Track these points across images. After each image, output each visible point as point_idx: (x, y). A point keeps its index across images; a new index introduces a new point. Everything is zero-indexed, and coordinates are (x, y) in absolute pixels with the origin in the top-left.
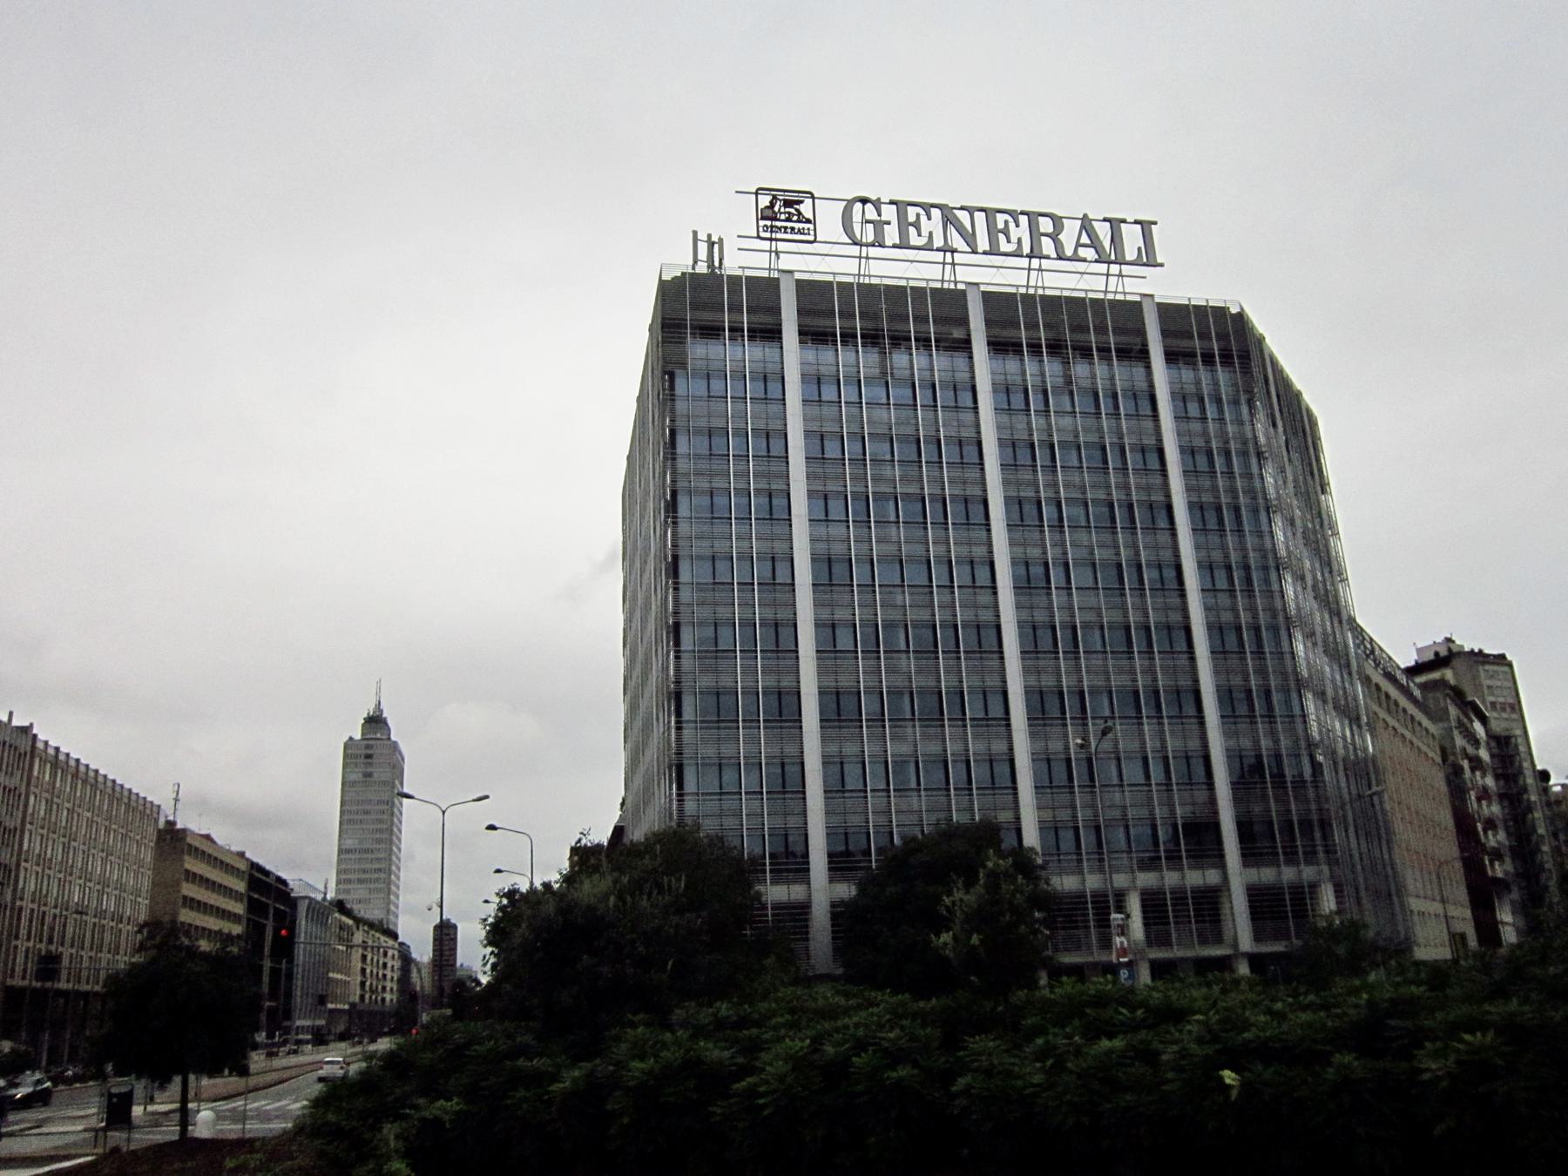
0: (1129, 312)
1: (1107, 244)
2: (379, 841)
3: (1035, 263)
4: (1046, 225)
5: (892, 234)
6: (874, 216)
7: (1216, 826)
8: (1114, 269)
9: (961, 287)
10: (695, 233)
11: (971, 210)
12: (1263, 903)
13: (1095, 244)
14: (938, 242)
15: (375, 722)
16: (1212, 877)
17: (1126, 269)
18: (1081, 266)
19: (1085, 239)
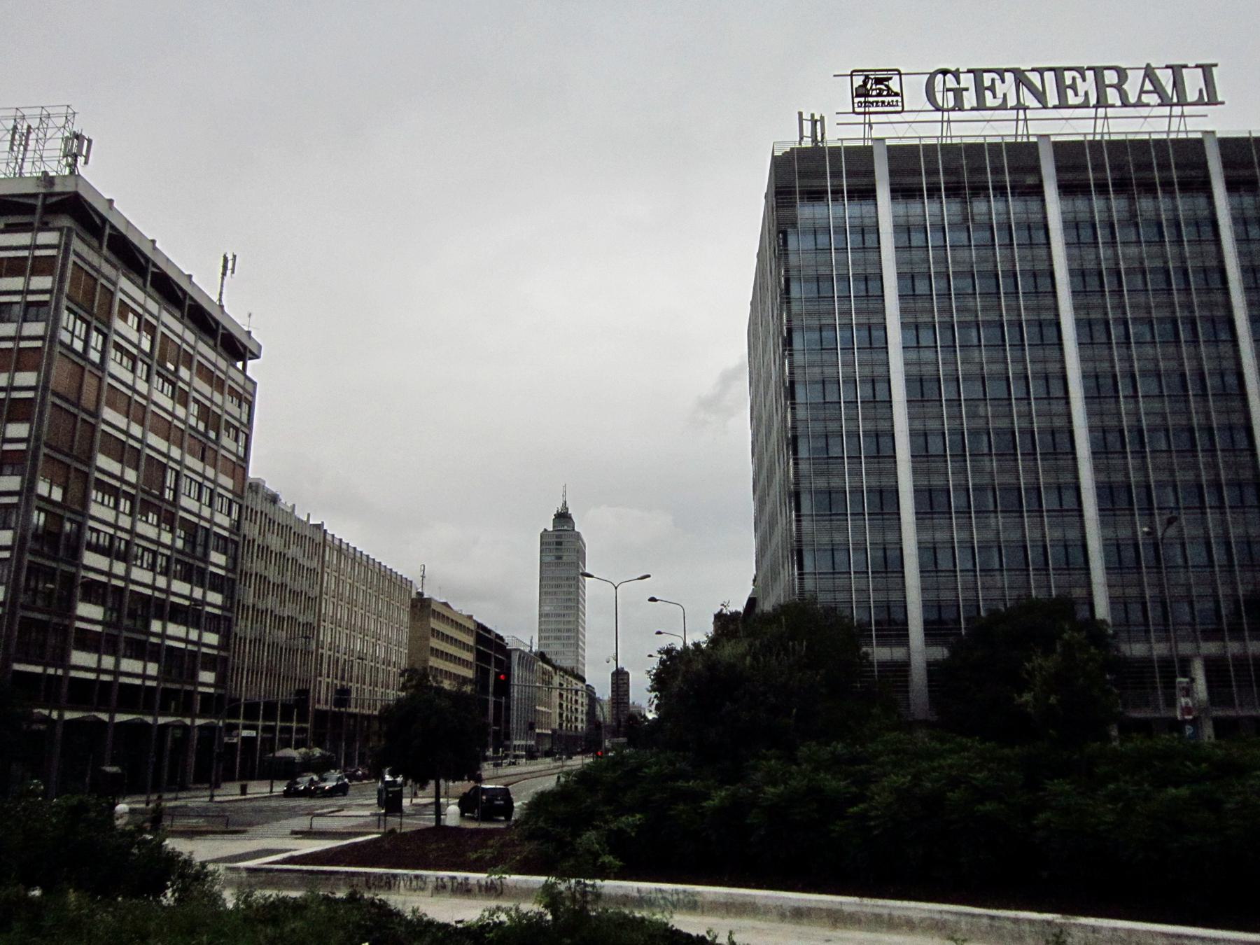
3: (1101, 111)
4: (1111, 77)
5: (970, 99)
8: (1177, 110)
11: (1041, 71)
13: (1158, 89)
14: (1012, 102)
15: (563, 517)
17: (1187, 110)
19: (1148, 86)
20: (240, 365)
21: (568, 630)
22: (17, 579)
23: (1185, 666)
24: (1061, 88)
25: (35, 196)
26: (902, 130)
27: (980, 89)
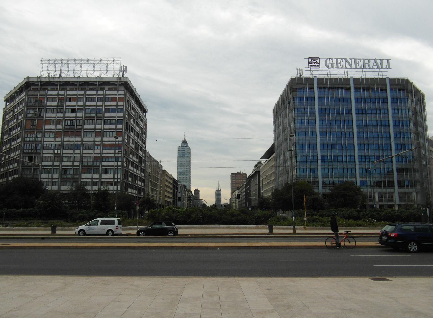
0: (383, 81)
1: (379, 64)
2: (187, 171)
3: (364, 70)
4: (367, 61)
5: (335, 65)
6: (331, 62)
7: (393, 182)
8: (381, 70)
9: (349, 77)
11: (351, 59)
12: (402, 196)
13: (377, 65)
14: (344, 67)
15: (184, 142)
16: (392, 190)
17: (383, 70)
18: (373, 70)
19: (375, 64)
20: (144, 114)
21: (186, 178)
22: (123, 173)
23: (374, 193)
24: (355, 63)
25: (117, 82)
26: (319, 72)
27: (337, 63)
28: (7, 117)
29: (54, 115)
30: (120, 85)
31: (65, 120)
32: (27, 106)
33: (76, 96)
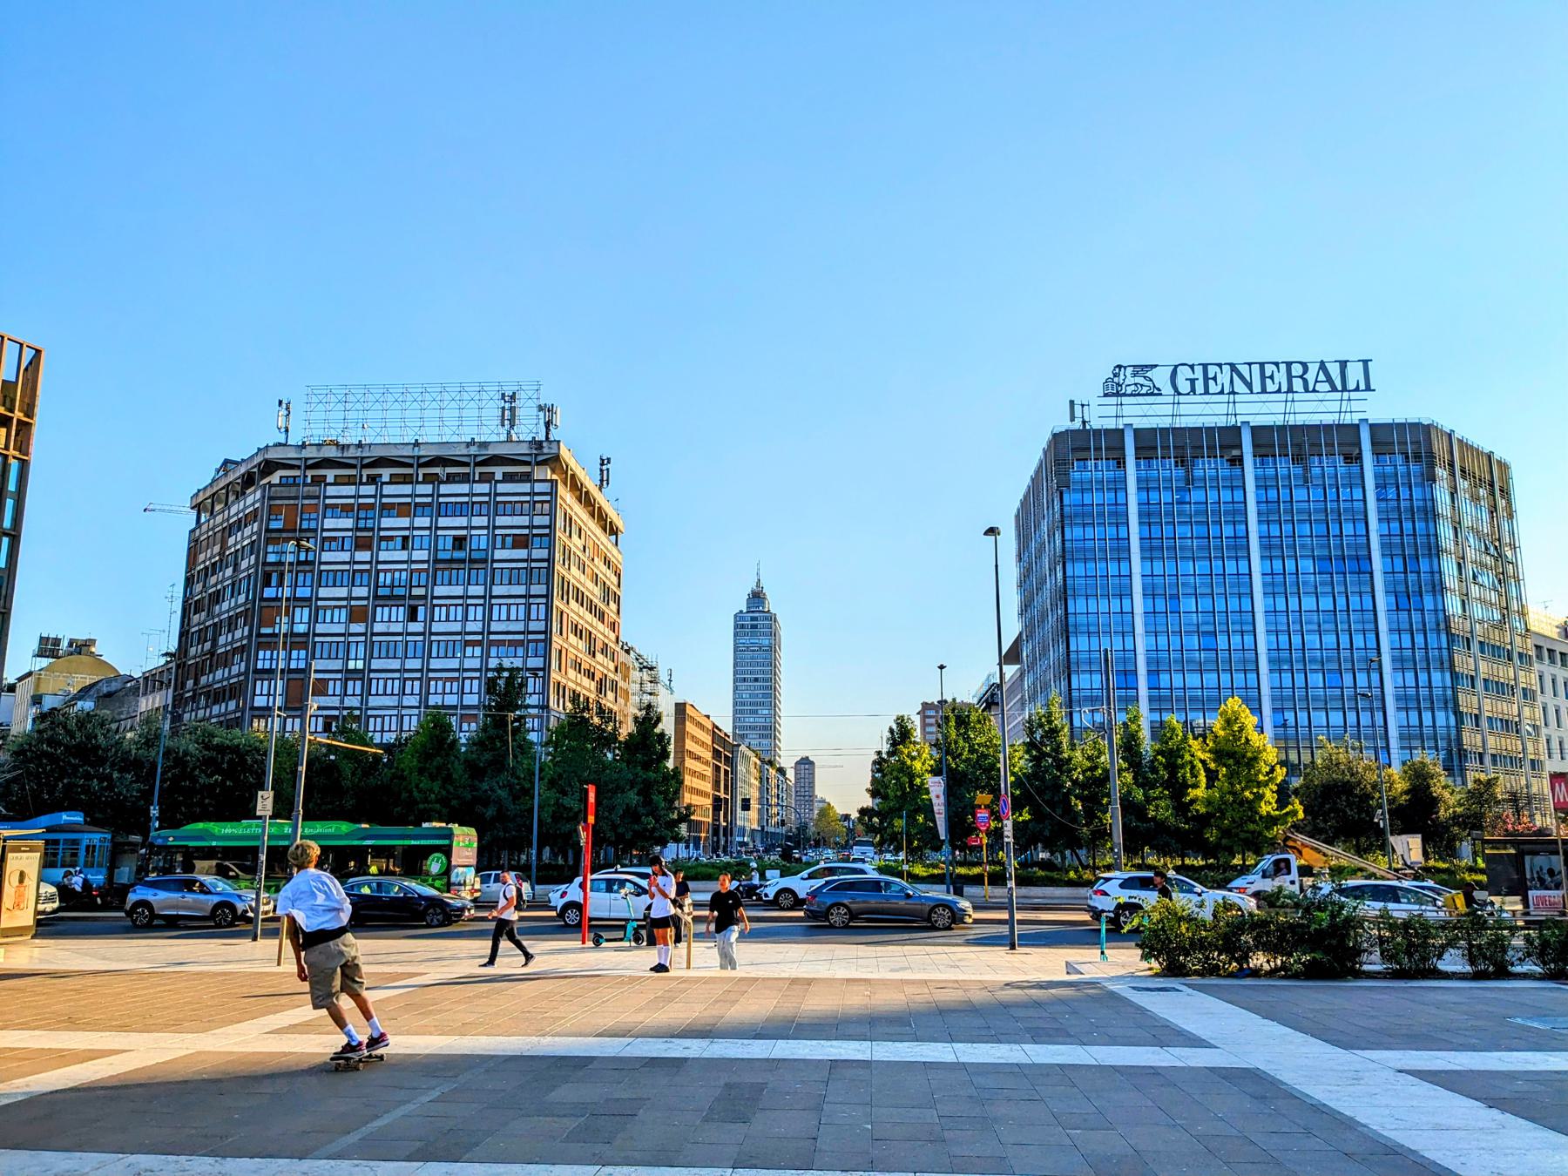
4: (1297, 370)
5: (1200, 387)
10: (1072, 402)
13: (1329, 380)
15: (757, 597)
18: (1320, 396)
19: (1322, 377)
28: (202, 557)
29: (345, 556)
30: (539, 464)
31: (378, 571)
32: (267, 530)
33: (408, 500)
